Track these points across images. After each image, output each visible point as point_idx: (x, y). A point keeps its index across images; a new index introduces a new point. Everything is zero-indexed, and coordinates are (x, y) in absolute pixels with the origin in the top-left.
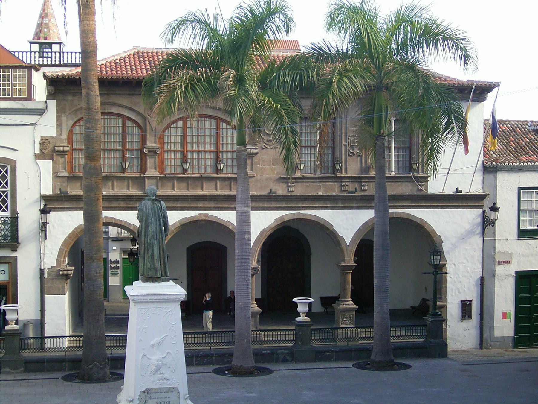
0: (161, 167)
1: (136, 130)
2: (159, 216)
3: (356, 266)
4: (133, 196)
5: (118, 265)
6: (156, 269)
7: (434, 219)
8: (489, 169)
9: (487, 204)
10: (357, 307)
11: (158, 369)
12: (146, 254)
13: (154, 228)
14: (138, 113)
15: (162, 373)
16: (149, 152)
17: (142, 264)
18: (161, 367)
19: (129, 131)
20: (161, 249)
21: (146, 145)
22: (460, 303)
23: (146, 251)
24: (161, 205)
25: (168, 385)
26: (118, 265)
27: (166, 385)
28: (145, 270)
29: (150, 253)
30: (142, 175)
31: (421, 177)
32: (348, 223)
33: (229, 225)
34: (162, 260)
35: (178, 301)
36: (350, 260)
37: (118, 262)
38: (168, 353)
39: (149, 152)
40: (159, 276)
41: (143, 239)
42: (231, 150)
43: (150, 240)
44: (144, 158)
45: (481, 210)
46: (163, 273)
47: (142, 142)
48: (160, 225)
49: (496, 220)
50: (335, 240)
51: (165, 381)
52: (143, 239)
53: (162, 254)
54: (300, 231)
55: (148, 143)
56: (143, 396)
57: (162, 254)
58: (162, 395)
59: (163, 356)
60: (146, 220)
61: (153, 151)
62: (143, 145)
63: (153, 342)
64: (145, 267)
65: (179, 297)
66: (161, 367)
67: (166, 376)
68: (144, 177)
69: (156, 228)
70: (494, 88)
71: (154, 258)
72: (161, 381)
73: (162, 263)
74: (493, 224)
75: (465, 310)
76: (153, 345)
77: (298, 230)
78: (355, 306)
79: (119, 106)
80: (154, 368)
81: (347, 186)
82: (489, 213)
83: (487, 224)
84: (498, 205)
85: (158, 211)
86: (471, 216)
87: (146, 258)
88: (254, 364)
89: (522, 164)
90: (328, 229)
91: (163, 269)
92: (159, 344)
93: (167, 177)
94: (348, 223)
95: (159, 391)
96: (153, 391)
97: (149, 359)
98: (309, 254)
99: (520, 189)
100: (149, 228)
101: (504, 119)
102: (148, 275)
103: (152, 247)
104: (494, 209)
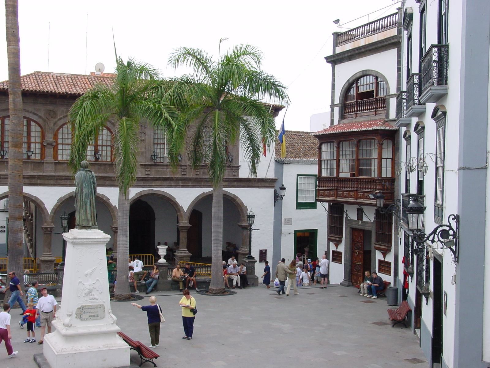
0: (56, 155)
1: (38, 129)
2: (91, 182)
3: (191, 227)
4: (35, 176)
5: (4, 229)
6: (88, 220)
7: (243, 195)
8: (280, 163)
9: (278, 185)
10: (191, 254)
11: (90, 292)
12: (81, 209)
13: (87, 191)
14: (40, 117)
15: (93, 295)
16: (48, 144)
17: (79, 217)
18: (92, 290)
19: (33, 129)
20: (92, 206)
21: (45, 139)
22: (259, 251)
23: (81, 207)
24: (92, 174)
25: (98, 303)
26: (4, 229)
27: (95, 303)
28: (81, 221)
29: (84, 208)
30: (42, 161)
31: (235, 167)
32: (185, 197)
33: (104, 197)
34: (92, 214)
35: (104, 243)
36: (185, 222)
37: (4, 227)
38: (98, 280)
39: (48, 144)
40: (90, 225)
41: (79, 198)
42: (106, 144)
43: (85, 199)
44: (44, 149)
45: (274, 189)
46: (93, 223)
47: (42, 137)
48: (91, 189)
49: (284, 196)
50: (176, 208)
51: (95, 300)
52: (79, 198)
53: (92, 209)
54: (148, 203)
55: (46, 138)
56: (79, 311)
57: (92, 209)
58: (92, 311)
59: (94, 283)
60: (81, 185)
61: (49, 144)
62: (42, 139)
63: (86, 272)
64: (81, 218)
65: (105, 240)
66: (92, 290)
67: (96, 296)
68: (44, 162)
69: (89, 191)
70: (283, 108)
71: (87, 212)
72: (92, 300)
73: (92, 216)
74: (281, 199)
75: (262, 256)
76: (87, 275)
77: (146, 203)
78: (190, 254)
79: (26, 111)
80: (87, 291)
81: (185, 171)
82: (279, 192)
83: (278, 198)
84: (285, 186)
85: (90, 179)
86: (269, 193)
87: (81, 212)
88: (131, 293)
89: (299, 159)
90: (172, 201)
91: (93, 220)
92: (91, 274)
93: (60, 163)
94: (185, 197)
95: (90, 307)
96: (86, 308)
97: (84, 284)
98: (154, 219)
99: (298, 175)
100: (84, 190)
101: (289, 130)
102: (83, 224)
103: (86, 204)
104: (283, 189)
